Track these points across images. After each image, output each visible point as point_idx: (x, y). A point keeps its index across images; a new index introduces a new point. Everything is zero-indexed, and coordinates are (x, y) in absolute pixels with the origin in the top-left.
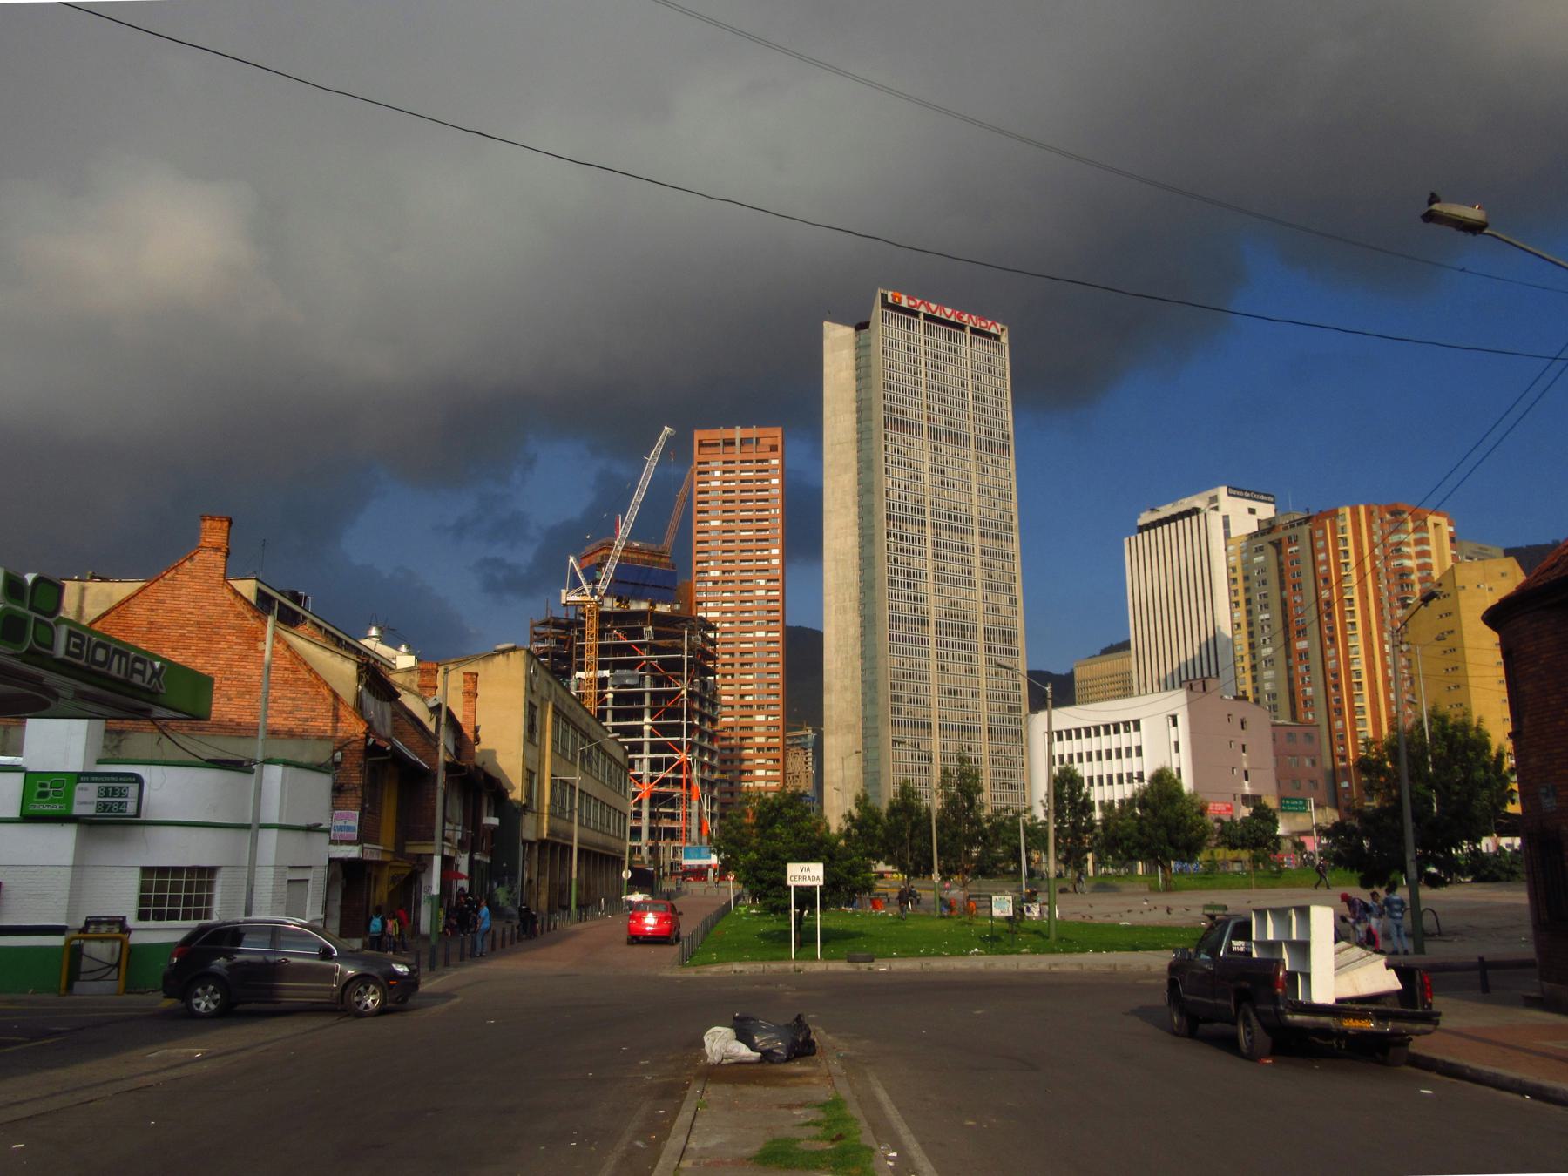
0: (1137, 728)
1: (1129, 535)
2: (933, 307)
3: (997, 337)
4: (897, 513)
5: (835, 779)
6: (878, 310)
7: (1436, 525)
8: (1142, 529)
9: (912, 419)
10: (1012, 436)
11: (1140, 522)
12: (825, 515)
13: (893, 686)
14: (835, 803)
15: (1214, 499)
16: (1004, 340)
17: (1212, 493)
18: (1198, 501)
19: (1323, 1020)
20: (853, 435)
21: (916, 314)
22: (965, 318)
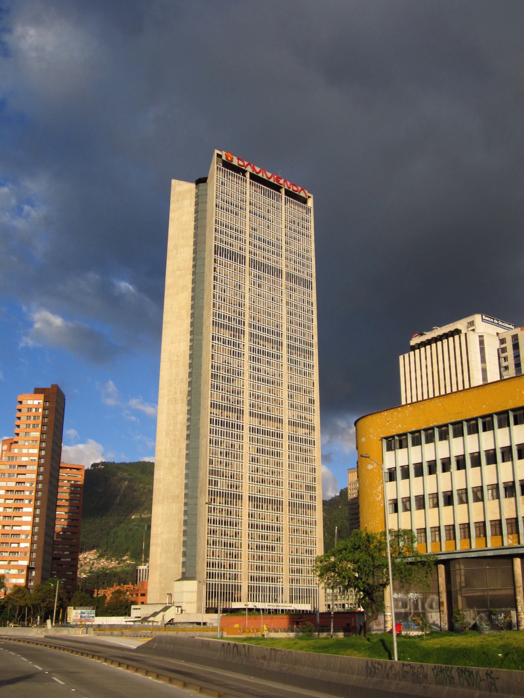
1: (403, 353)
2: (258, 169)
3: (305, 201)
4: (221, 321)
5: (159, 541)
6: (215, 165)
8: (413, 348)
10: (314, 275)
11: (413, 342)
12: (164, 325)
13: (211, 462)
14: (159, 562)
15: (472, 324)
16: (310, 203)
17: (469, 319)
18: (461, 325)
19: (131, 653)
21: (244, 172)
22: (282, 181)
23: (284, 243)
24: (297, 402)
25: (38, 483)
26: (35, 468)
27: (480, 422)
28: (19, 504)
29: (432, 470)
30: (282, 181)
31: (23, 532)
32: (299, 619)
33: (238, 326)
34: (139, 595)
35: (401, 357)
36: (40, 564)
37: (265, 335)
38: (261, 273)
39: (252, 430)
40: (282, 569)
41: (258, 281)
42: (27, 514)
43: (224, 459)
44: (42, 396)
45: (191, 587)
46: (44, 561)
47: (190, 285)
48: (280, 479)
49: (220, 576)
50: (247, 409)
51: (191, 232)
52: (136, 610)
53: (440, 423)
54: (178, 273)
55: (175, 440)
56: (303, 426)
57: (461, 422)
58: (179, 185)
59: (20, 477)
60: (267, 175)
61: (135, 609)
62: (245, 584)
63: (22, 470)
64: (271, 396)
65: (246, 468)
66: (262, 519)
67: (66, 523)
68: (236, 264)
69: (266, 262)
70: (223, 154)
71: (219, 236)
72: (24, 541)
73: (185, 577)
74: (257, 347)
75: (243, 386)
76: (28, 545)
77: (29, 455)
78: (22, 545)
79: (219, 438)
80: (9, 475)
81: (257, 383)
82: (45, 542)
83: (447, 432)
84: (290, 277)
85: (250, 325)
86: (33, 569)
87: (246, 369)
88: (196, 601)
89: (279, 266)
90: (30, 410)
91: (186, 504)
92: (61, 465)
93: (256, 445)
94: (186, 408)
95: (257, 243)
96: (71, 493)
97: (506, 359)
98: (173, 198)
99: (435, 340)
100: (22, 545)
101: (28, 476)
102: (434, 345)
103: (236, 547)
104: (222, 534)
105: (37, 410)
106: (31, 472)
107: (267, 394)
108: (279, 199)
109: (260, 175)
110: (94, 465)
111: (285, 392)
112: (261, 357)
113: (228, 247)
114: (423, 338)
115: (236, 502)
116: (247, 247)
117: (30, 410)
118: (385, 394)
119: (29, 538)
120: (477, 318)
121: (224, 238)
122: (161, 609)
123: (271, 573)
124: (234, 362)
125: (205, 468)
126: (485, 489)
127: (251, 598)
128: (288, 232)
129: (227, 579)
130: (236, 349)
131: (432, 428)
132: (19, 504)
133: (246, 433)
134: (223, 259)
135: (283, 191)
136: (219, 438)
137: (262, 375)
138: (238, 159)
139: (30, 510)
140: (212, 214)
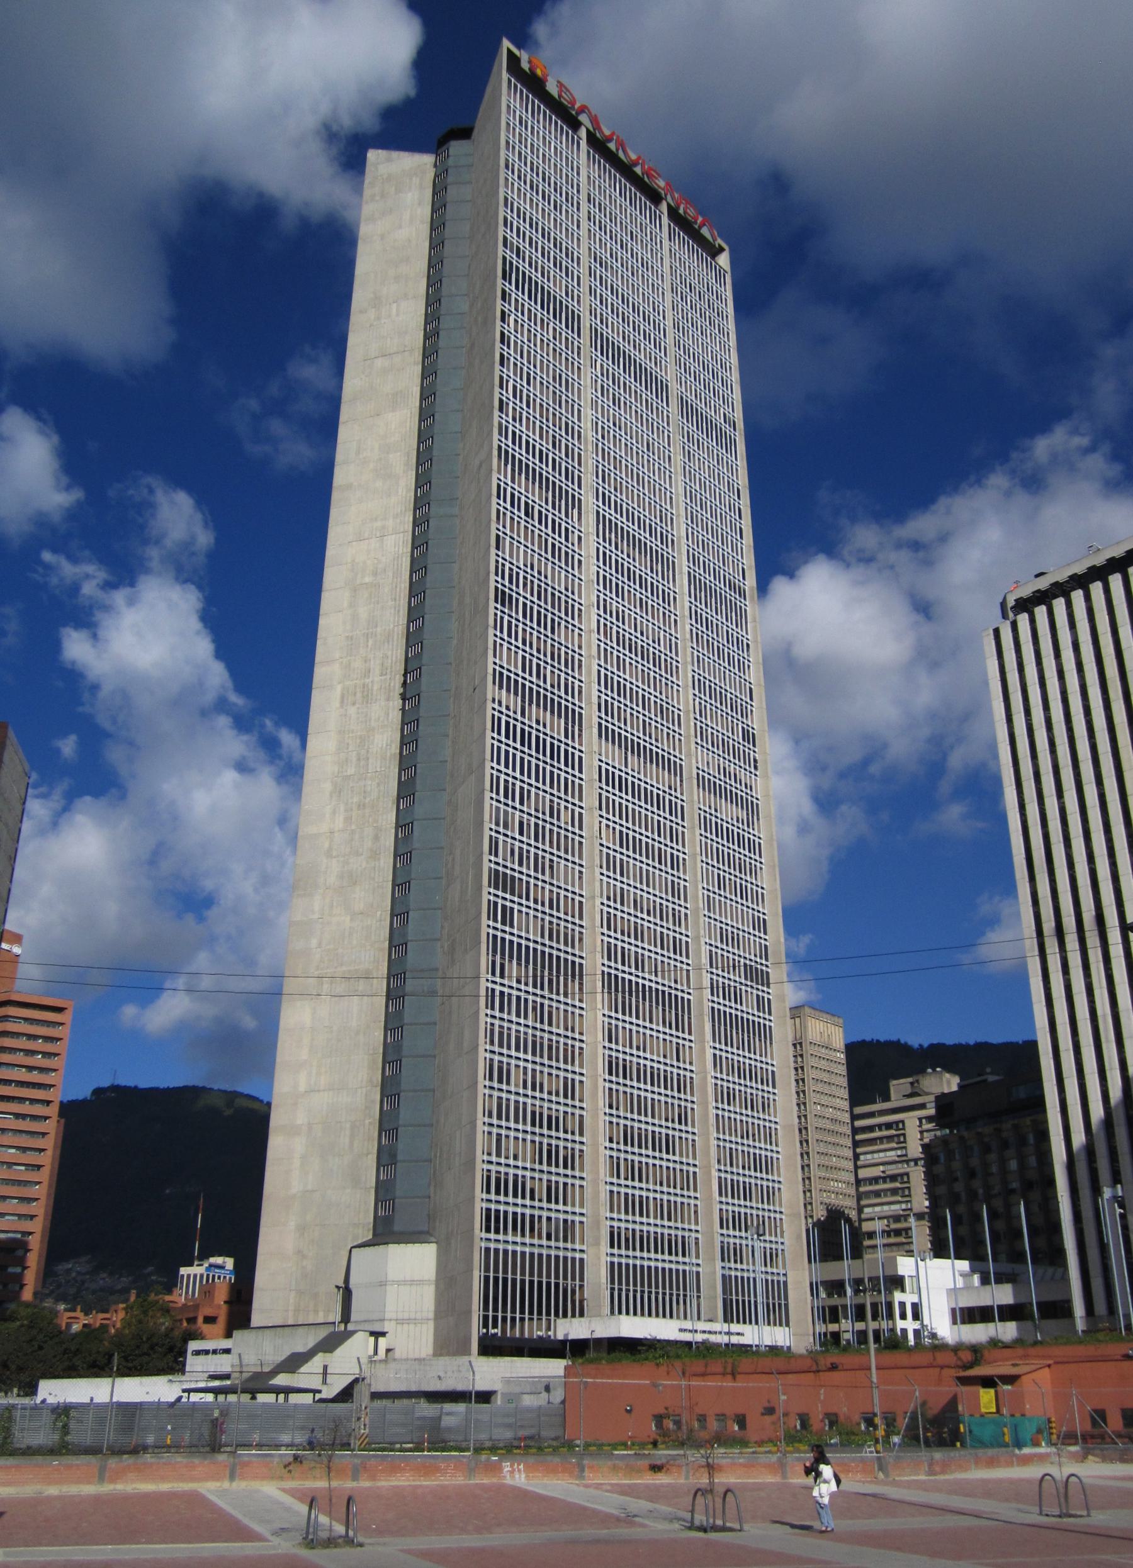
5: (301, 1119)
14: (296, 1187)
32: (966, 1367)
34: (200, 1320)
39: (607, 777)
40: (696, 1212)
45: (413, 1264)
49: (518, 1224)
50: (592, 717)
51: (421, 265)
52: (202, 1358)
54: (379, 363)
55: (361, 806)
56: (733, 798)
58: (389, 160)
61: (197, 1353)
62: (597, 1260)
65: (593, 889)
66: (638, 1049)
73: (385, 1231)
75: (580, 647)
88: (431, 1315)
103: (566, 1132)
104: (525, 1082)
110: (98, 1092)
115: (566, 985)
122: (311, 1343)
123: (666, 1223)
127: (618, 1306)
129: (540, 1237)
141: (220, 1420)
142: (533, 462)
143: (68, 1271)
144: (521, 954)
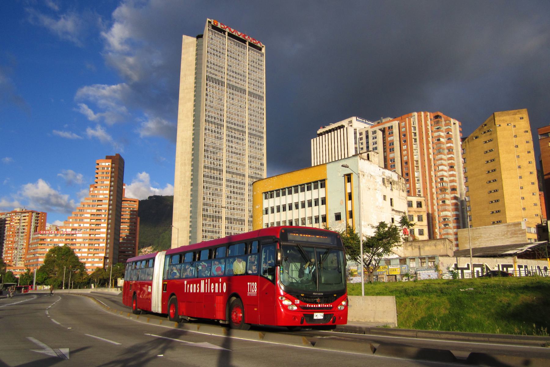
0: (323, 186)
1: (313, 138)
2: (233, 30)
4: (210, 119)
7: (454, 124)
8: (321, 134)
9: (220, 78)
10: (265, 93)
11: (319, 132)
13: (204, 199)
15: (351, 122)
16: (263, 50)
17: (349, 119)
18: (345, 123)
20: (193, 85)
23: (247, 74)
24: (253, 165)
25: (109, 210)
26: (107, 201)
27: (306, 186)
28: (98, 222)
29: (316, 203)
30: (247, 37)
31: (101, 238)
33: (219, 122)
35: (312, 140)
36: (112, 256)
37: (236, 127)
38: (234, 92)
41: (231, 96)
42: (103, 228)
43: (211, 197)
44: (111, 160)
46: (114, 253)
47: (193, 98)
48: (243, 207)
50: (224, 169)
53: (289, 186)
54: (186, 91)
55: (185, 186)
57: (297, 186)
59: (99, 206)
60: (238, 34)
63: (100, 203)
64: (239, 162)
67: (128, 232)
68: (221, 86)
69: (237, 85)
70: (212, 21)
71: (209, 70)
72: (102, 243)
74: (231, 134)
76: (104, 245)
77: (103, 194)
78: (101, 245)
79: (209, 185)
80: (92, 206)
81: (230, 154)
82: (114, 243)
83: (291, 190)
84: (250, 94)
85: (227, 122)
86: (108, 258)
87: (224, 147)
89: (244, 88)
90: (103, 168)
91: (191, 222)
92: (123, 199)
93: (229, 189)
94: (190, 168)
95: (232, 74)
96: (131, 215)
97: (362, 144)
98: (183, 46)
99: (330, 131)
100: (101, 245)
101: (104, 206)
102: (324, 136)
105: (108, 168)
106: (105, 204)
107: (236, 161)
108: (245, 48)
109: (234, 34)
110: (150, 197)
111: (247, 159)
112: (233, 139)
113: (214, 77)
114: (324, 130)
116: (226, 76)
117: (103, 168)
118: (303, 161)
119: (105, 241)
120: (354, 119)
121: (212, 71)
124: (218, 142)
125: (201, 201)
126: (306, 219)
128: (249, 67)
130: (219, 135)
131: (285, 189)
132: (98, 222)
133: (224, 182)
134: (211, 84)
135: (247, 43)
136: (209, 185)
137: (234, 150)
138: (221, 24)
139: (105, 225)
140: (205, 57)
141: (475, 287)
142: (213, 120)
143: (145, 251)
144: (210, 216)
